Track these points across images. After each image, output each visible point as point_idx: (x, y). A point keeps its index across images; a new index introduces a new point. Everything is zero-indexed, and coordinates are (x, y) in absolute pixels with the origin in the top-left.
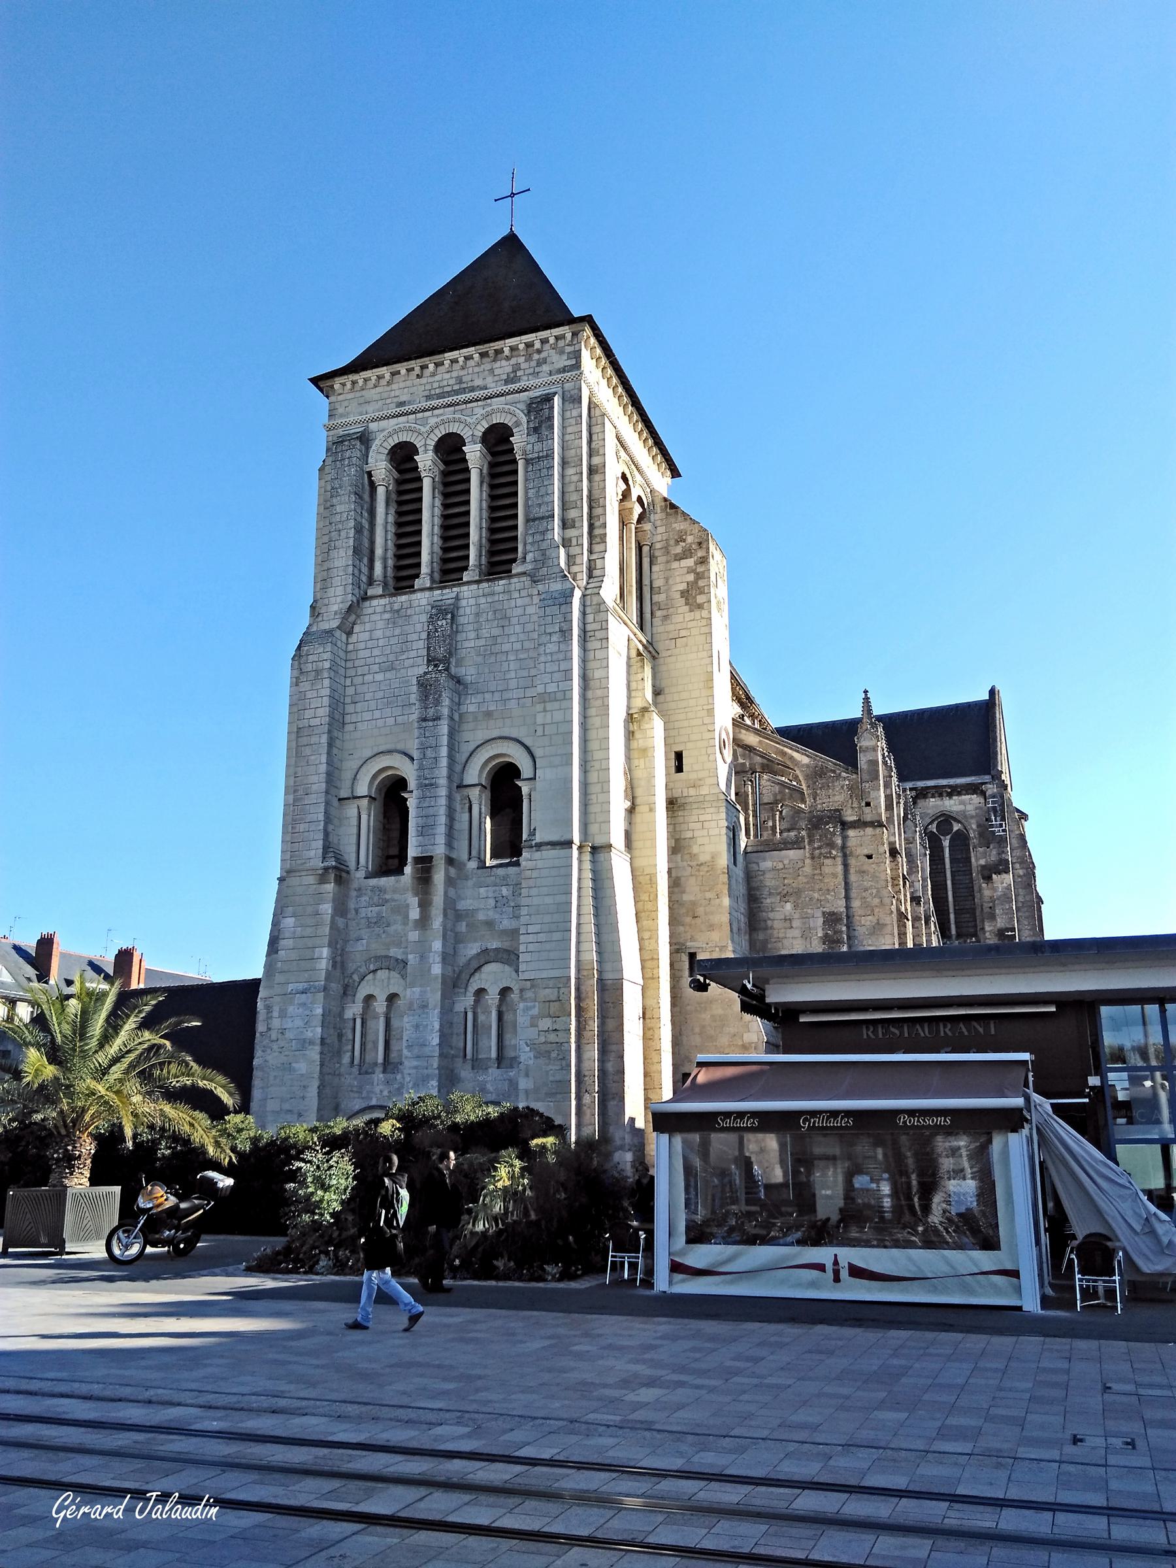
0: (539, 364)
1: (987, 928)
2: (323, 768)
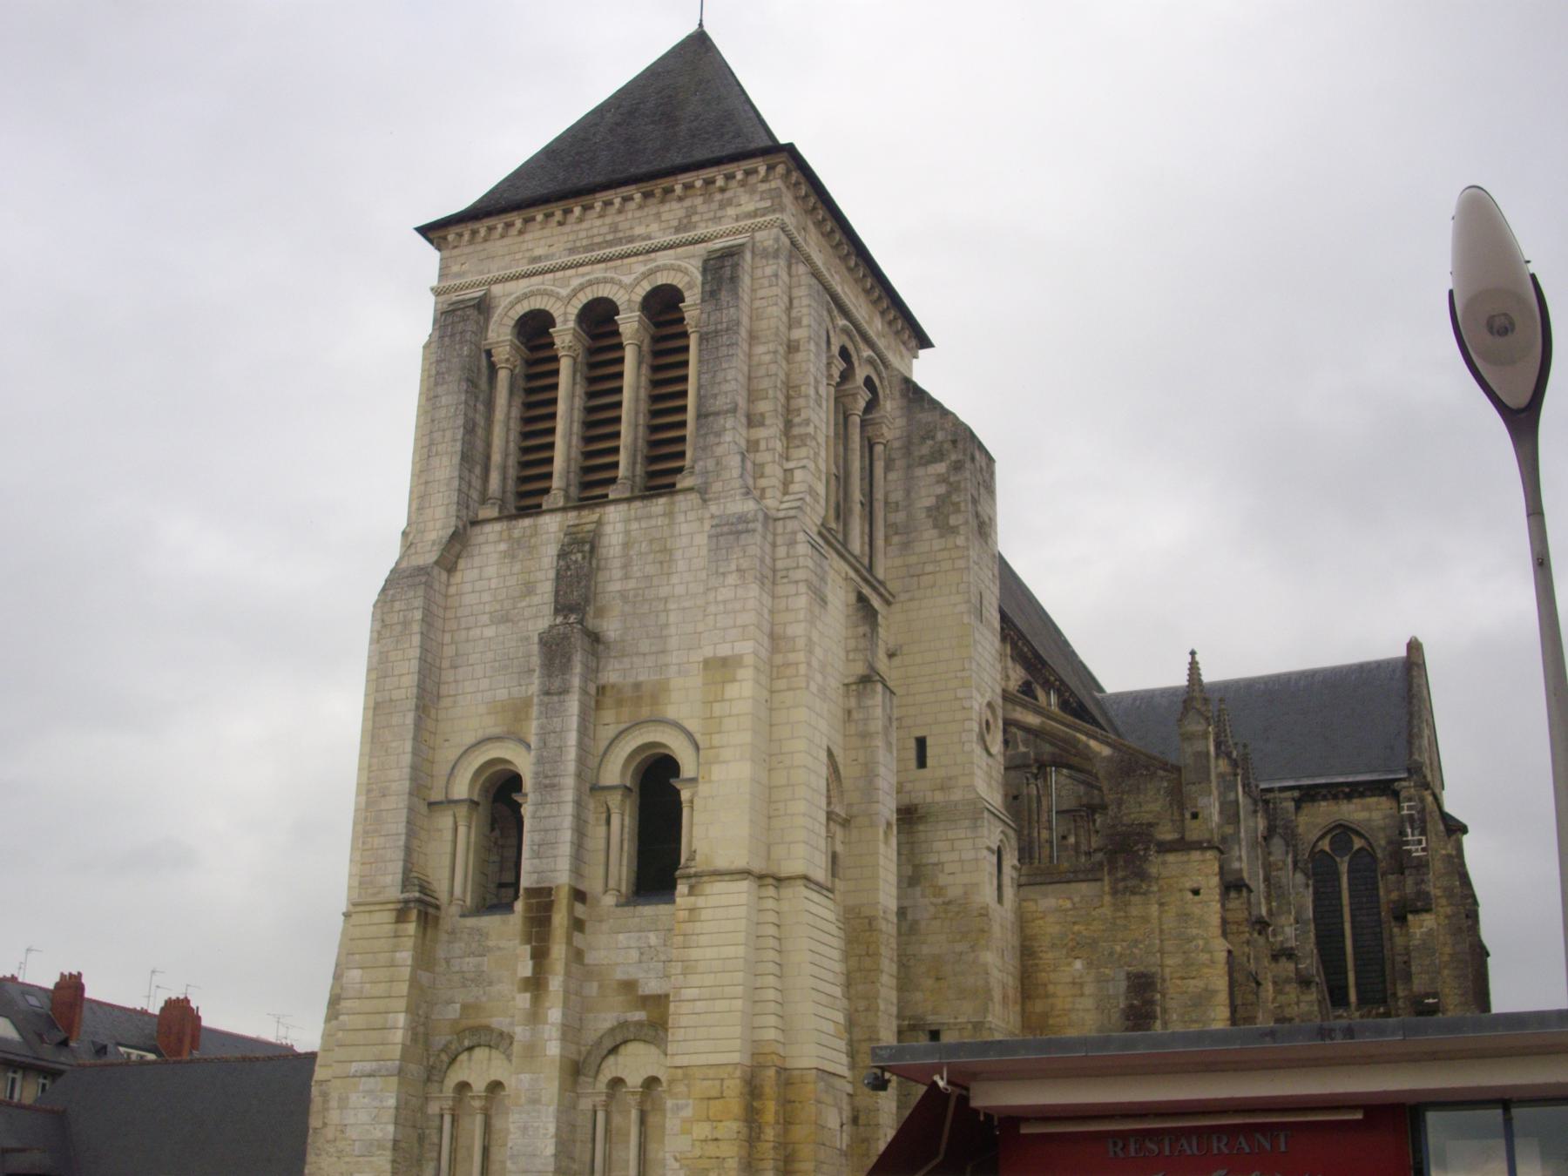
0: (722, 206)
1: (1401, 994)
2: (407, 759)
